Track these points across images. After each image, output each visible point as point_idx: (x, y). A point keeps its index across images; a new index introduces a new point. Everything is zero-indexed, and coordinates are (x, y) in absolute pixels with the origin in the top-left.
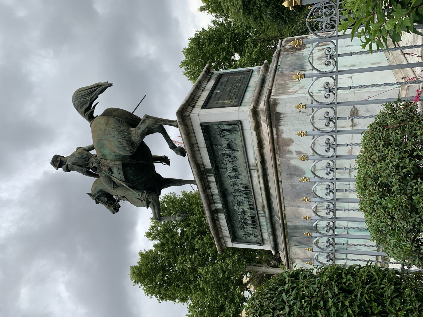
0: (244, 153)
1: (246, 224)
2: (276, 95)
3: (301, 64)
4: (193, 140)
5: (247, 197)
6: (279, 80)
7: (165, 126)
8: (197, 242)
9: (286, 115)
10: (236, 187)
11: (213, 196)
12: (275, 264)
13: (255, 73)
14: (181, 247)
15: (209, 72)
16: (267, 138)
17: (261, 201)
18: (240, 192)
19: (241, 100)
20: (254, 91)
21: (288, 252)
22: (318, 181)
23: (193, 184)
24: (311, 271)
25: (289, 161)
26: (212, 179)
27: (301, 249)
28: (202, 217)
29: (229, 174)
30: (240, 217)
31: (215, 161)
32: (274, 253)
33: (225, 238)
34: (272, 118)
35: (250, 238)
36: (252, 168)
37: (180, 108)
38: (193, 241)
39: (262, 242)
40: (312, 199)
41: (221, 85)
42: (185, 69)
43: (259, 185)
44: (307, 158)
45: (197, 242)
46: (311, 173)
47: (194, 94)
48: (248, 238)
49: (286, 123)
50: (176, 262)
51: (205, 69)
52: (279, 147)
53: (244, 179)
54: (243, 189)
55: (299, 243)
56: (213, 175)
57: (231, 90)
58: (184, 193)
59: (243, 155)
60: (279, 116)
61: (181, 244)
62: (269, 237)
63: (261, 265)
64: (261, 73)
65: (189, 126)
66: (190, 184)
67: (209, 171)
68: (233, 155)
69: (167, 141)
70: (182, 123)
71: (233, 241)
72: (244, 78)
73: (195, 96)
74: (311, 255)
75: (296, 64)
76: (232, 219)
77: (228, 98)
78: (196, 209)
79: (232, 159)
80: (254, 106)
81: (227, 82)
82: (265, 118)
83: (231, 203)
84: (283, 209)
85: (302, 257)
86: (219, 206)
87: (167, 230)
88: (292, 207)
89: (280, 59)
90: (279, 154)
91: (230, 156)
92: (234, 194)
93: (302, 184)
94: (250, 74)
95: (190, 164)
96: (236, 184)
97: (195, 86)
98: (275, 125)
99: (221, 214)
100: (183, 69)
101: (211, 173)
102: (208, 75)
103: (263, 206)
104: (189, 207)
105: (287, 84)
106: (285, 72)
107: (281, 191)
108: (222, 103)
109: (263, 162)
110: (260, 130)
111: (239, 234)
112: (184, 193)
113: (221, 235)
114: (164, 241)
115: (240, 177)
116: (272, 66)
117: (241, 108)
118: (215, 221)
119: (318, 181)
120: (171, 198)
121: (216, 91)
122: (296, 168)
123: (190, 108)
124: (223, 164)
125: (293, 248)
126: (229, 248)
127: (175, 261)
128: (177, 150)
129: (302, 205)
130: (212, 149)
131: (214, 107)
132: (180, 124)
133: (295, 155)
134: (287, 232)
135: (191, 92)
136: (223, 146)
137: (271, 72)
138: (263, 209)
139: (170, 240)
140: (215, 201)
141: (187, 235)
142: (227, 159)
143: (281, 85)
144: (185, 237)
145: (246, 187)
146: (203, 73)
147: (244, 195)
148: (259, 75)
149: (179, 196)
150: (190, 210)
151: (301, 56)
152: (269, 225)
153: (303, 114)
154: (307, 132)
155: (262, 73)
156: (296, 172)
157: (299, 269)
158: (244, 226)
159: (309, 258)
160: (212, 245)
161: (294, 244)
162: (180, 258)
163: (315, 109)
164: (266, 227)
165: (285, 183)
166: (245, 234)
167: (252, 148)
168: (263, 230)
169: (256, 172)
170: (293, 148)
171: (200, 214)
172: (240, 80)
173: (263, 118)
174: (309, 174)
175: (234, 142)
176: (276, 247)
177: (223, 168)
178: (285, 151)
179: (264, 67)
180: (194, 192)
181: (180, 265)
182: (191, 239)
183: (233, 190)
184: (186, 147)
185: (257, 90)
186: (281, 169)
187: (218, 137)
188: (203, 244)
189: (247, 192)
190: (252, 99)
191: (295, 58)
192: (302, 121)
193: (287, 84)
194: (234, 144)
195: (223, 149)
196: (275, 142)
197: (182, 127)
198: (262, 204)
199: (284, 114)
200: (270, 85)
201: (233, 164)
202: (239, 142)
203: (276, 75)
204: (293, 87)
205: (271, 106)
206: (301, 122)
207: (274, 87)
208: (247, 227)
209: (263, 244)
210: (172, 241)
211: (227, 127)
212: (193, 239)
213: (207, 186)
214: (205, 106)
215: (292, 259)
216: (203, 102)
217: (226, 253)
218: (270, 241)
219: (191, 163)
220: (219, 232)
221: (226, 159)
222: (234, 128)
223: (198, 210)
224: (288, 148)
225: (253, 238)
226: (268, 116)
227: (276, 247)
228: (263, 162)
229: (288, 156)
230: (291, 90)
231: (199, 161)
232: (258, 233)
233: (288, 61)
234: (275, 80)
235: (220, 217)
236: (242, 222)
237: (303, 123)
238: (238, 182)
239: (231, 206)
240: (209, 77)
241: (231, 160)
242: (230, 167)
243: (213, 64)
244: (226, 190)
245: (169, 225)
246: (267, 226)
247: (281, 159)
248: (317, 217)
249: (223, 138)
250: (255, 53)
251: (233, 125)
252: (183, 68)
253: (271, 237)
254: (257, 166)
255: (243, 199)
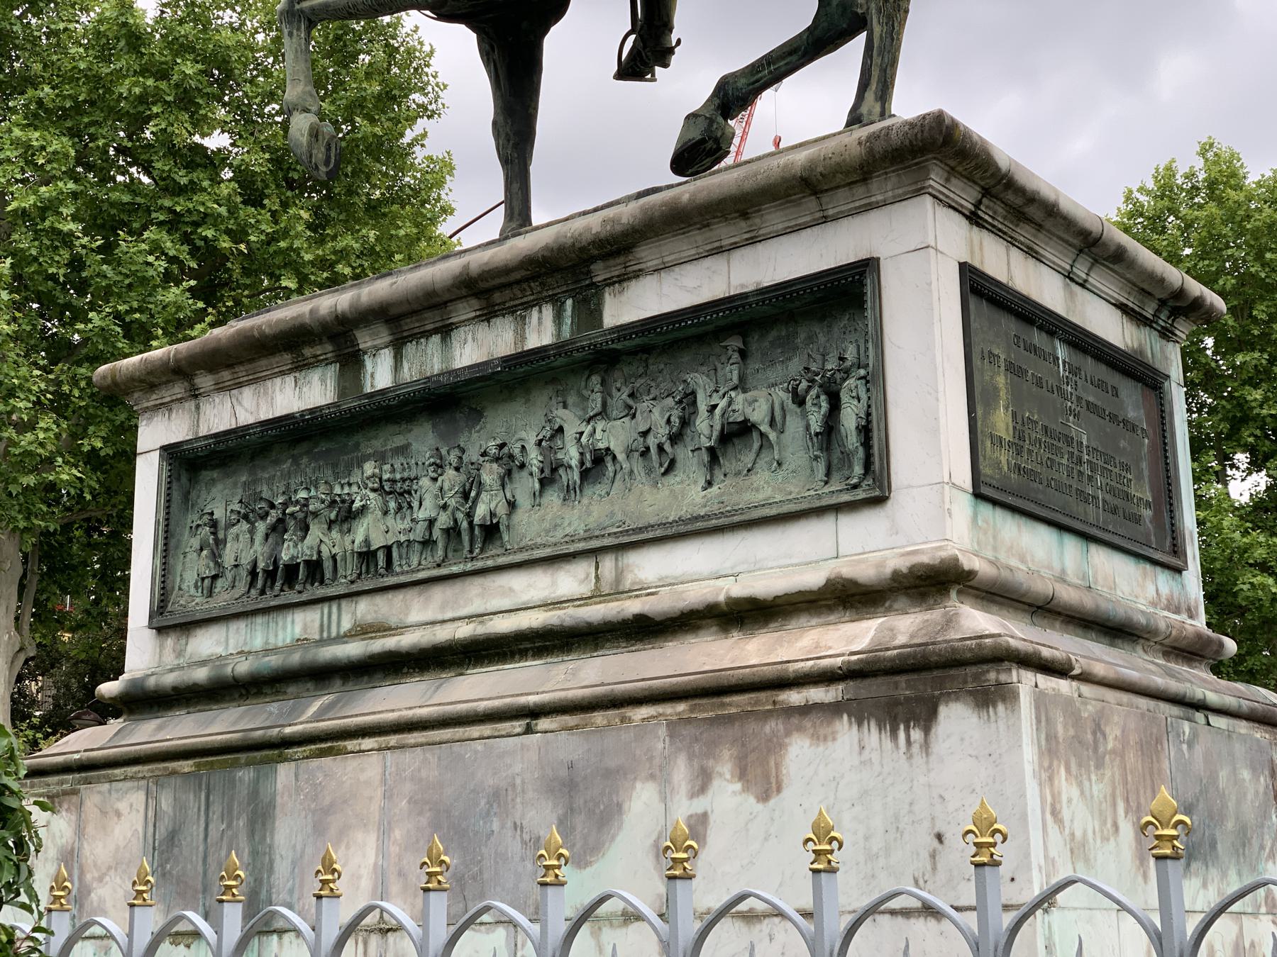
0: (697, 518)
1: (278, 529)
2: (1041, 700)
3: (1213, 845)
4: (774, 219)
5: (437, 534)
6: (1123, 715)
7: (855, 48)
8: (156, 248)
9: (919, 759)
10: (490, 474)
11: (436, 339)
12: (34, 703)
13: (1163, 582)
14: (120, 150)
15: (1176, 313)
16: (782, 654)
17: (415, 616)
18: (466, 495)
19: (1010, 500)
20: (1062, 579)
21: (118, 772)
22: (544, 932)
23: (509, 216)
24: (23, 898)
25: (652, 777)
26: (541, 330)
27: (137, 846)
28: (303, 281)
29: (570, 432)
30: (316, 497)
31: (646, 350)
32: (108, 689)
33: (191, 405)
34: (902, 679)
35: (192, 556)
36: (608, 563)
37: (967, 135)
38: (160, 224)
39: (168, 622)
40: (439, 903)
41: (1101, 385)
42: (1190, 176)
43: (506, 603)
44: (678, 874)
45: (156, 248)
46: (588, 899)
47: (1048, 224)
48: (195, 542)
49: (875, 757)
50: (33, 121)
51: (1196, 288)
52: (730, 719)
53: (541, 519)
54: (481, 511)
55: (172, 838)
56: (566, 333)
57: (1069, 440)
58: (440, 171)
59: (684, 511)
60: (917, 720)
61: (137, 155)
62: (203, 663)
63: (28, 619)
64: (1164, 619)
65: (860, 190)
66: (509, 201)
67: (590, 311)
68: (683, 453)
69: (768, 60)
70: (879, 147)
71: (171, 452)
72: (1137, 519)
73: (1039, 227)
74: (102, 900)
75: (1215, 817)
76: (305, 446)
77: (1021, 425)
78: (347, 241)
79: (660, 448)
80: (971, 574)
81: (1113, 418)
82: (901, 639)
83: (399, 441)
84: (368, 743)
85: (87, 849)
86: (380, 374)
87: (222, 67)
88: (379, 792)
89: (1243, 727)
90: (689, 721)
91: (675, 438)
92: (453, 458)
93: (514, 846)
94: (1157, 556)
95: (629, 199)
96: (509, 473)
97: (1095, 228)
98: (863, 694)
99: (331, 384)
100: (1190, 163)
101: (578, 325)
102: (1164, 308)
103: (382, 629)
104: (360, 201)
105: (1100, 765)
106: (1170, 753)
107: (475, 731)
108: (996, 389)
109: (643, 630)
110: (830, 609)
111: (217, 491)
112: (440, 171)
113: (205, 381)
114: (156, 49)
115: (553, 498)
116: (1199, 682)
117: (964, 503)
118: (293, 348)
119: (544, 932)
120: (407, 90)
121: (1062, 352)
122: (606, 817)
123: (966, 195)
124: (632, 395)
125: (138, 798)
126: (131, 431)
127: (38, 116)
128: (711, 121)
129: (394, 849)
130: (720, 333)
131: (975, 339)
132: (874, 137)
133: (683, 809)
134: (235, 765)
135: (1065, 206)
136: (739, 398)
137: (1170, 674)
138: (363, 631)
139: (163, 85)
140: (410, 349)
141: (193, 188)
142: (658, 418)
143: (1098, 729)
144: (182, 178)
145: (491, 531)
146: (1174, 275)
147: (444, 520)
148: (1154, 604)
149: (420, 140)
150: (346, 208)
151: (1262, 847)
152: (274, 661)
153: (925, 855)
154: (833, 871)
155: (1162, 625)
156: (588, 809)
157: (29, 827)
158: (264, 517)
159: (84, 891)
160: (139, 336)
161: (166, 803)
162: (55, 146)
163: (970, 920)
164: (258, 643)
165: (518, 756)
166: (214, 524)
167: (726, 568)
168: (240, 626)
169: (586, 589)
170: (727, 798)
171: (322, 263)
172: (1128, 497)
173: (902, 628)
174: (579, 888)
175: (761, 463)
176: (144, 702)
177: (607, 394)
178: (711, 750)
179: (1199, 636)
180: (444, 228)
181: (16, 143)
182: (171, 211)
183: (473, 455)
184: (735, 174)
185: (1068, 595)
186: (600, 730)
187: (795, 366)
188: (144, 281)
189: (466, 538)
190: (1014, 562)
191: (1250, 815)
192: (887, 850)
193: (1100, 765)
194: (748, 459)
195: (717, 396)
196: (762, 695)
197: (856, 151)
198: (393, 621)
199: (926, 746)
200: (1099, 670)
201: (629, 452)
202: (765, 486)
203: (1152, 703)
204: (1083, 800)
205: (971, 674)
206: (877, 844)
207: (1086, 689)
208: (259, 537)
209: (161, 630)
210: (158, 97)
211: (849, 419)
212: (173, 223)
213: (497, 297)
214: (977, 287)
215: (75, 792)
216: (1002, 278)
217: (90, 420)
218: (179, 668)
219: (634, 206)
220: (226, 375)
221: (657, 416)
222: (847, 457)
223: (343, 254)
224: (725, 767)
225: (192, 568)
226: (914, 655)
227: (144, 702)
228: (643, 630)
229: (681, 772)
230: (1068, 789)
231: (647, 254)
232: (223, 598)
233: (1234, 771)
234: (1125, 697)
235: (315, 376)
236: (285, 505)
237: (872, 857)
238: (524, 486)
239: (377, 444)
240: (1149, 312)
241: (652, 441)
242: (614, 435)
243: (1209, 342)
244: (476, 415)
245: (252, 81)
246: (267, 651)
247: (662, 731)
248: (564, 927)
249: (787, 398)
250: (1264, 587)
251: (861, 452)
252: (1199, 163)
253: (201, 675)
254: (618, 593)
255: (422, 515)
